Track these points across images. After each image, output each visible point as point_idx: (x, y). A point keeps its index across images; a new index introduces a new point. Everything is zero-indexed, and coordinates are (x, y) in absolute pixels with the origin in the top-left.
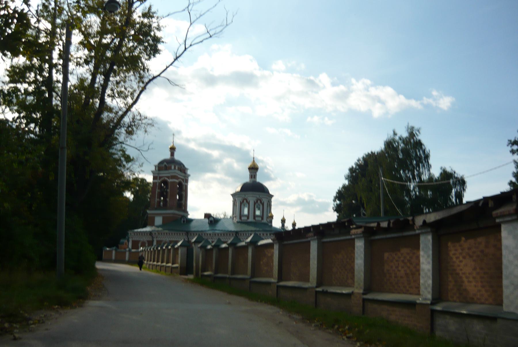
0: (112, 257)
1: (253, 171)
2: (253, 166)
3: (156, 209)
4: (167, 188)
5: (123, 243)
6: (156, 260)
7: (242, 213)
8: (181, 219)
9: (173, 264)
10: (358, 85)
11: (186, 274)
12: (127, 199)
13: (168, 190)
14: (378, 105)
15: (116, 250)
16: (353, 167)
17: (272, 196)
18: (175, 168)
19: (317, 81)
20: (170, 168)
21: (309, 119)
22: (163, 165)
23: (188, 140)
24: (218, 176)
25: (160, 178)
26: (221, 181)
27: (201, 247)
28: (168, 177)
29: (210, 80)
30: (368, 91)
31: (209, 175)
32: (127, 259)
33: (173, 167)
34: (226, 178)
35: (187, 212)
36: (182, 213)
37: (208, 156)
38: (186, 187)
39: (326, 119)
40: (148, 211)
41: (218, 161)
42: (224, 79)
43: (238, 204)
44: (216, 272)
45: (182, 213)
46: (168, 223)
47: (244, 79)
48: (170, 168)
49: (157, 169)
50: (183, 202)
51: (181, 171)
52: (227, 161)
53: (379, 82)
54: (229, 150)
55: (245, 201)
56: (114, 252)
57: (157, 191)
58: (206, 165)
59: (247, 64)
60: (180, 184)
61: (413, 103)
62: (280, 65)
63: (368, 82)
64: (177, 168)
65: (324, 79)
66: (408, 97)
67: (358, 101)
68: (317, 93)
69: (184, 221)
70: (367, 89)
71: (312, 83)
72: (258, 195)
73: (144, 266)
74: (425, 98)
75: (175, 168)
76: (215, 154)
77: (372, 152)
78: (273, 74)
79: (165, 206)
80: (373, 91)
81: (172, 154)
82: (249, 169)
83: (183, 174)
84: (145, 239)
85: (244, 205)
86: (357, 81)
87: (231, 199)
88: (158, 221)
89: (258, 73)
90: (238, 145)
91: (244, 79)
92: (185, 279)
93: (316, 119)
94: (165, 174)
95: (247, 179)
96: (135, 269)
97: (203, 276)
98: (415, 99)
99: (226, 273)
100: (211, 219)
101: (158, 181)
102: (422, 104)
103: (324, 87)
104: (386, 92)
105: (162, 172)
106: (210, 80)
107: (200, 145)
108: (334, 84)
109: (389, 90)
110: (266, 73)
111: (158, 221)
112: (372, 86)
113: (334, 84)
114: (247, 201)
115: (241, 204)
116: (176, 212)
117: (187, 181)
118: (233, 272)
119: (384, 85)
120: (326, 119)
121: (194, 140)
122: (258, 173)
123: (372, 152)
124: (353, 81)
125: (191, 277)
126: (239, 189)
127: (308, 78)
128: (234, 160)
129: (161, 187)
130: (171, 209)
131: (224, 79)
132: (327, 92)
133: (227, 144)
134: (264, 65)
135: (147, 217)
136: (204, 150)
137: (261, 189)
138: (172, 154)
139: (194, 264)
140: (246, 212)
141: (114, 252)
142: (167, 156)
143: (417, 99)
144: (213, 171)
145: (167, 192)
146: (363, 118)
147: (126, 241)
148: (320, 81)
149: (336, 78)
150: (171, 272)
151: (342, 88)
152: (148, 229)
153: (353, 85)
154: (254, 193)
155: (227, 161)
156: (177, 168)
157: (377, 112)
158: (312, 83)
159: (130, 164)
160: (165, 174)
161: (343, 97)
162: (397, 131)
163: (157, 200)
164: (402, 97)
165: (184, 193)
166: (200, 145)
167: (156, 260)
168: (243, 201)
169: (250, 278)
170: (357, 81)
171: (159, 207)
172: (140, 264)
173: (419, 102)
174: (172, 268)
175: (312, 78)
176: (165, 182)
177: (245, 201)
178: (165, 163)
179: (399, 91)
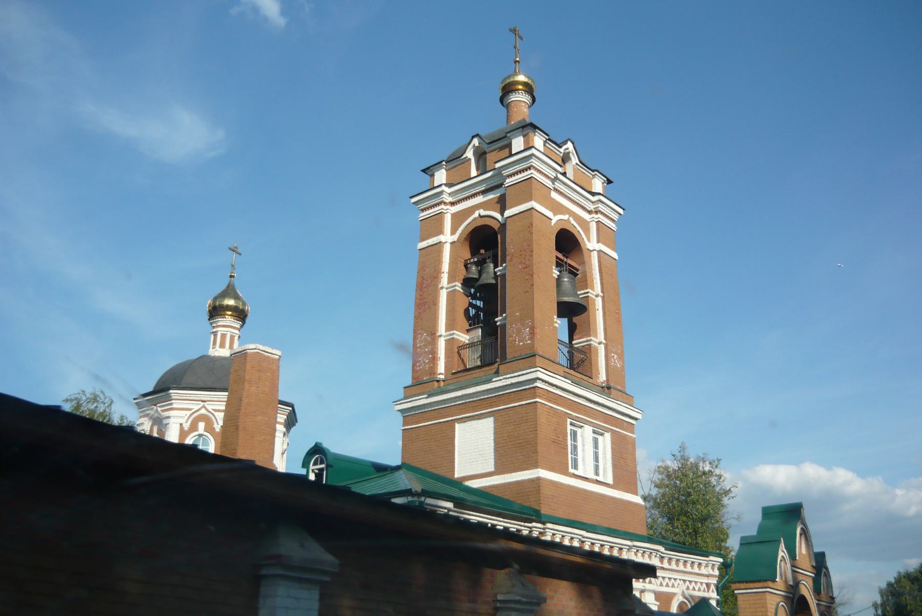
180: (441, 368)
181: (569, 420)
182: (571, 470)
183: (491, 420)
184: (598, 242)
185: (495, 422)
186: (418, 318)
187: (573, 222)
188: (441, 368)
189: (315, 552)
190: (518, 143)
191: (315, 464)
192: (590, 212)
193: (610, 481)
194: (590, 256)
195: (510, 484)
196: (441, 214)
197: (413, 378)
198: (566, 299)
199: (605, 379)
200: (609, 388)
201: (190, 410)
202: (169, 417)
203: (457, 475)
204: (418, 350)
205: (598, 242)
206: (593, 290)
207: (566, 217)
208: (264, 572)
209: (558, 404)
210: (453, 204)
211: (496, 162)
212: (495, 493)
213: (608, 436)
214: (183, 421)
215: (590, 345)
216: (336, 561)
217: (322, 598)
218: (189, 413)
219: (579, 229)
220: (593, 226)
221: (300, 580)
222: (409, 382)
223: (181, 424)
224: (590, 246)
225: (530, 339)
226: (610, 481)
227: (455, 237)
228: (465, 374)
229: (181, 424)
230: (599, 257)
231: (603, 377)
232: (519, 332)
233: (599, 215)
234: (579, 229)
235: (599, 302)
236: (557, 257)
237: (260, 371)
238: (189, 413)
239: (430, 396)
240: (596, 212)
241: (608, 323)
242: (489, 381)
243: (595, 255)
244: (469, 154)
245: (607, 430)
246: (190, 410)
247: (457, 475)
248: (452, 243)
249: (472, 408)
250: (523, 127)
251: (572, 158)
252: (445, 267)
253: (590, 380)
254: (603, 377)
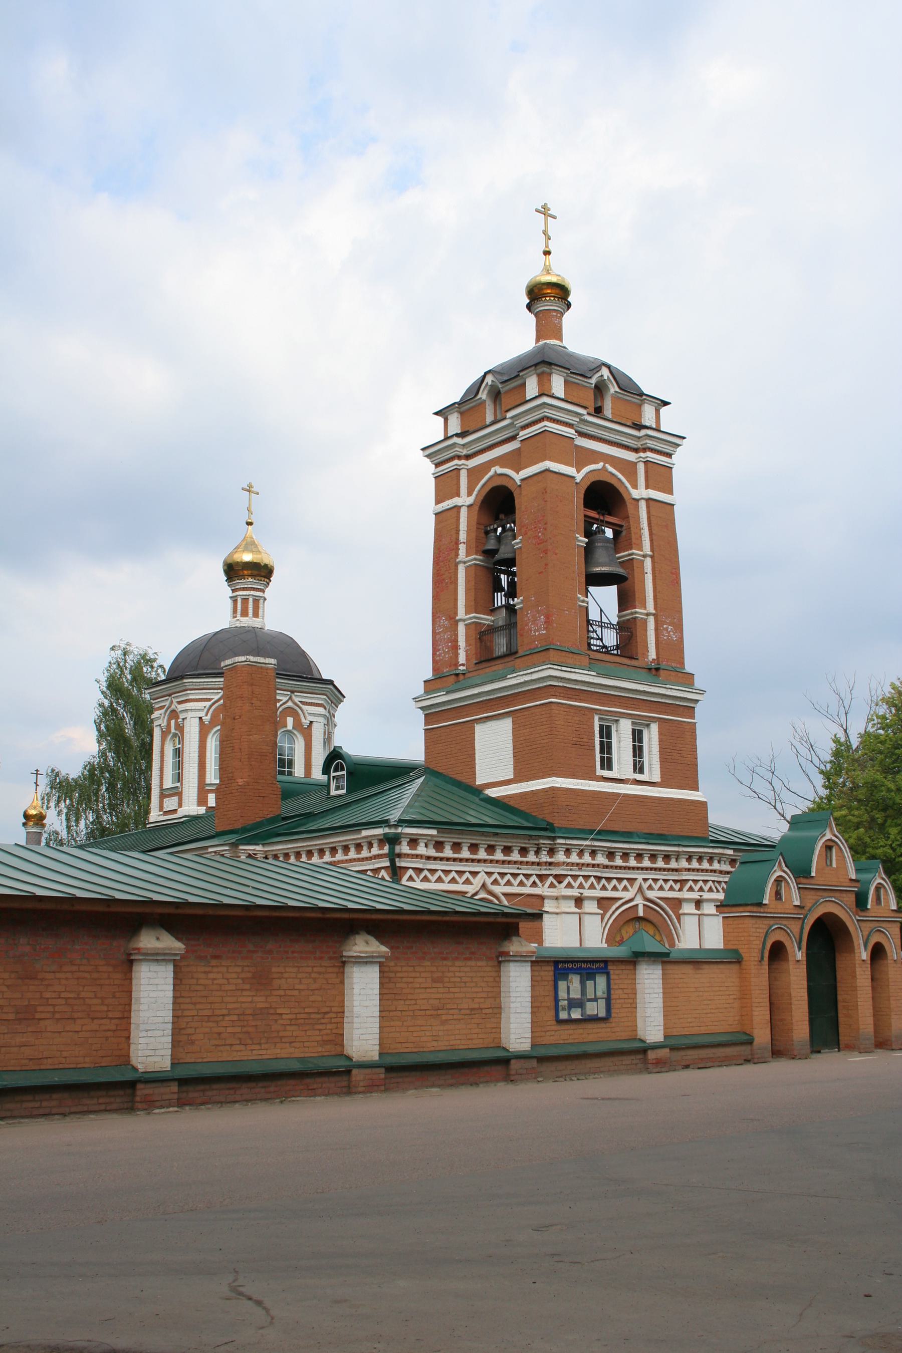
180: (462, 659)
181: (596, 718)
182: (600, 772)
183: (507, 725)
184: (647, 487)
185: (514, 723)
186: (436, 597)
187: (610, 469)
188: (462, 659)
189: (168, 942)
190: (532, 387)
191: (336, 770)
192: (636, 450)
193: (657, 778)
194: (637, 508)
195: (525, 793)
196: (457, 470)
197: (434, 670)
198: (597, 569)
199: (655, 657)
200: (657, 669)
201: (210, 700)
202: (186, 711)
203: (479, 782)
204: (438, 637)
205: (647, 487)
206: (641, 549)
207: (600, 466)
208: (133, 957)
209: (581, 701)
210: (468, 457)
211: (507, 411)
212: (512, 803)
213: (654, 727)
214: (202, 714)
215: (635, 618)
216: (183, 946)
217: (175, 966)
218: (208, 704)
219: (620, 476)
220: (641, 468)
221: (157, 960)
222: (429, 675)
223: (200, 718)
224: (635, 494)
225: (546, 629)
226: (657, 778)
227: (470, 500)
228: (488, 664)
229: (200, 718)
230: (648, 507)
231: (652, 655)
232: (534, 621)
233: (649, 454)
234: (620, 476)
235: (648, 564)
236: (585, 516)
237: (252, 685)
238: (208, 704)
239: (448, 693)
240: (645, 450)
241: (658, 588)
242: (503, 678)
243: (643, 505)
244: (483, 395)
245: (654, 720)
246: (210, 700)
247: (479, 782)
248: (469, 506)
249: (491, 707)
250: (536, 365)
251: (610, 386)
252: (463, 536)
253: (634, 663)
254: (652, 655)
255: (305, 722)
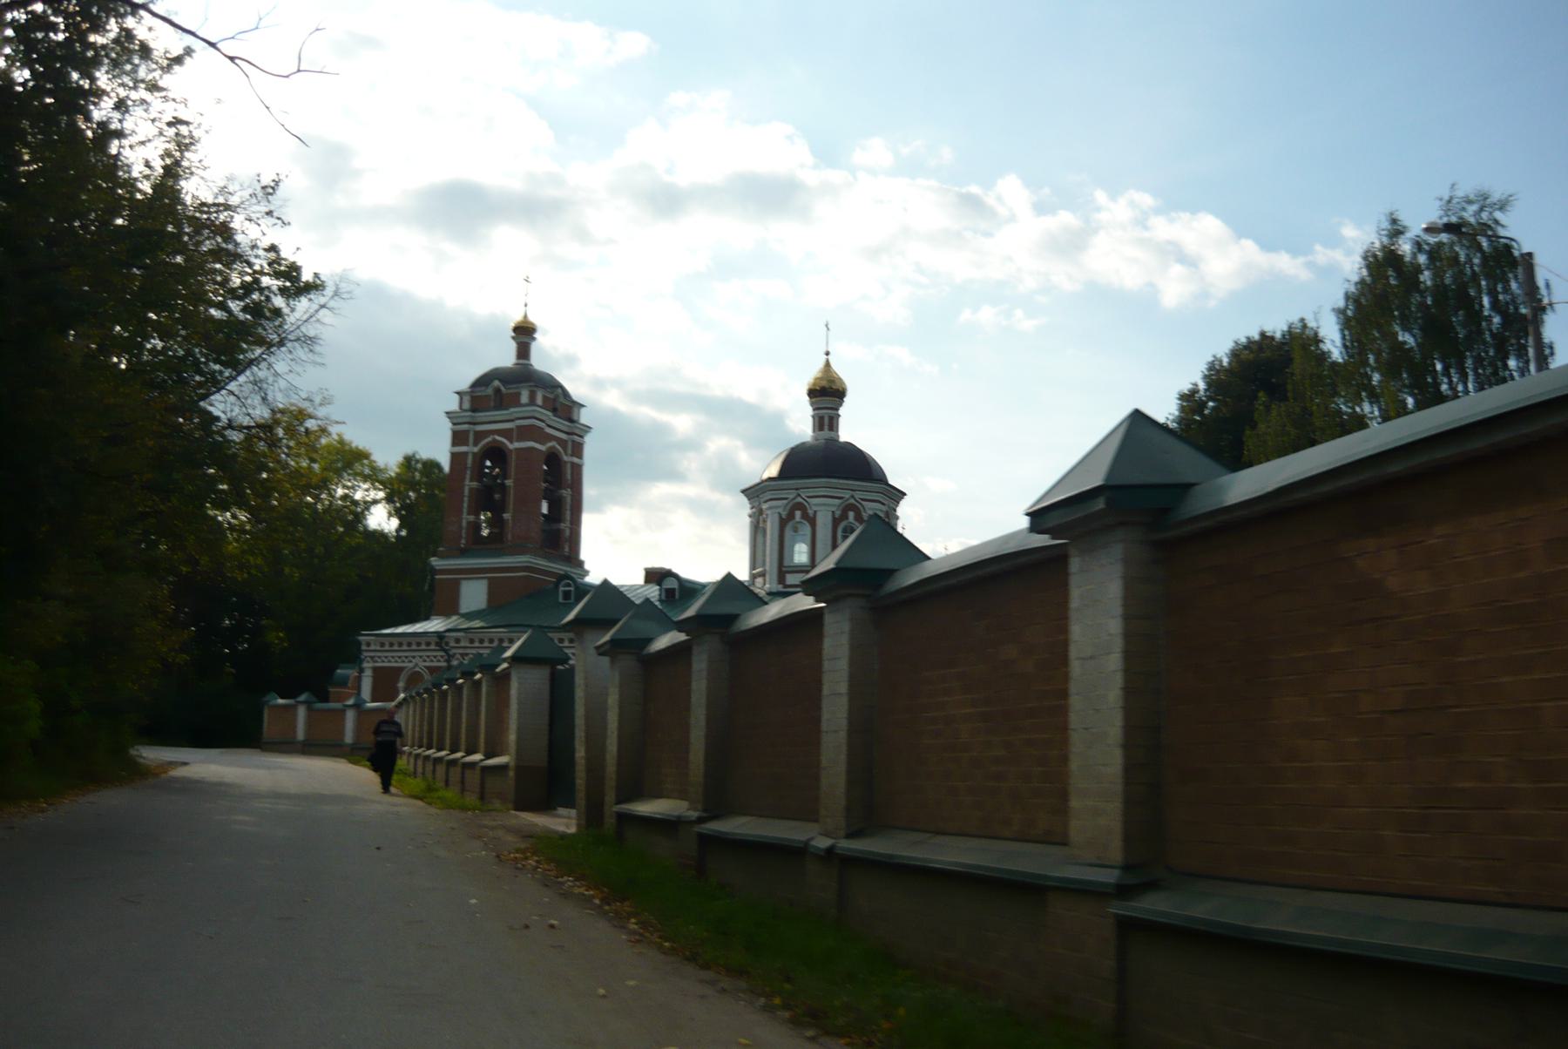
0: (342, 732)
1: (827, 401)
2: (824, 383)
3: (463, 553)
4: (505, 475)
5: (343, 683)
6: (448, 742)
7: (786, 563)
8: (557, 585)
9: (488, 756)
10: (1117, 210)
11: (545, 805)
12: (379, 536)
13: (509, 482)
14: (1177, 269)
15: (310, 709)
16: (1194, 392)
17: (899, 495)
18: (532, 401)
19: (990, 200)
20: (514, 401)
21: (966, 315)
22: (490, 391)
23: (598, 384)
24: (690, 490)
25: (479, 436)
26: (698, 507)
27: (614, 649)
28: (506, 433)
29: (666, 201)
30: (1146, 228)
31: (661, 489)
32: (349, 738)
33: (524, 398)
34: (716, 496)
35: (580, 564)
36: (559, 568)
37: (661, 429)
38: (577, 470)
39: (1019, 313)
40: (435, 562)
41: (690, 445)
42: (708, 196)
43: (771, 526)
44: (717, 802)
45: (559, 568)
46: (510, 600)
47: (770, 196)
48: (514, 401)
49: (467, 405)
50: (565, 526)
51: (554, 411)
52: (718, 444)
53: (1176, 201)
54: (725, 411)
55: (798, 514)
56: (302, 712)
57: (469, 484)
58: (652, 458)
59: (777, 151)
60: (553, 459)
61: (1284, 262)
62: (875, 152)
63: (1146, 200)
64: (539, 401)
65: (1011, 192)
66: (1267, 246)
67: (1115, 259)
68: (988, 234)
69: (567, 595)
70: (1141, 222)
71: (973, 204)
72: (850, 490)
73: (401, 763)
74: (1318, 248)
75: (532, 401)
76: (682, 423)
77: (1263, 334)
78: (855, 178)
79: (496, 544)
80: (1163, 229)
81: (523, 352)
82: (812, 393)
83: (563, 424)
84: (419, 662)
85: (796, 530)
86: (1113, 197)
87: (742, 512)
88: (474, 595)
89: (811, 178)
90: (750, 397)
91: (770, 196)
92: (528, 835)
93: (987, 315)
94: (495, 422)
95: (801, 426)
96: (363, 777)
97: (625, 819)
98: (1288, 251)
99: (808, 812)
100: (670, 584)
101: (471, 449)
102: (1310, 265)
103: (1012, 218)
104: (1202, 231)
105: (481, 416)
106: (666, 201)
107: (636, 397)
108: (1041, 209)
109: (1210, 224)
110: (835, 176)
111: (474, 595)
112: (1158, 211)
113: (1041, 209)
114: (805, 516)
115: (783, 523)
116: (542, 563)
117: (578, 450)
118: (867, 814)
119: (1194, 209)
120: (1019, 313)
121: (618, 383)
122: (846, 412)
123: (1263, 334)
124: (1101, 196)
125: (564, 822)
126: (773, 471)
127: (964, 190)
128: (739, 443)
129: (479, 473)
130: (519, 550)
131: (708, 196)
132: (1020, 235)
133: (718, 392)
134: (827, 155)
135: (433, 579)
136: (647, 412)
137: (856, 468)
138: (523, 352)
139: (580, 753)
140: (800, 554)
141: (302, 712)
142: (506, 357)
143: (1294, 251)
144: (674, 476)
145: (503, 487)
146: (1138, 308)
147: (352, 673)
148: (999, 198)
149: (1047, 191)
150: (482, 797)
151: (1066, 218)
152: (435, 625)
153: (1099, 209)
154: (827, 477)
155: (718, 444)
156: (539, 401)
157: (1174, 290)
158: (973, 204)
159: (303, 304)
160: (495, 422)
161: (1070, 245)
162: (1405, 218)
163: (467, 518)
164: (1249, 245)
165: (566, 493)
166: (636, 397)
167: (448, 742)
168: (791, 516)
169: (1123, 891)
170: (1113, 197)
171: (477, 545)
172: (382, 759)
173: (1301, 260)
174: (486, 769)
175: (974, 189)
176: (497, 453)
177: (798, 514)
178: (496, 383)
179: (1241, 229)
227: (476, 450)
255: (810, 512)
